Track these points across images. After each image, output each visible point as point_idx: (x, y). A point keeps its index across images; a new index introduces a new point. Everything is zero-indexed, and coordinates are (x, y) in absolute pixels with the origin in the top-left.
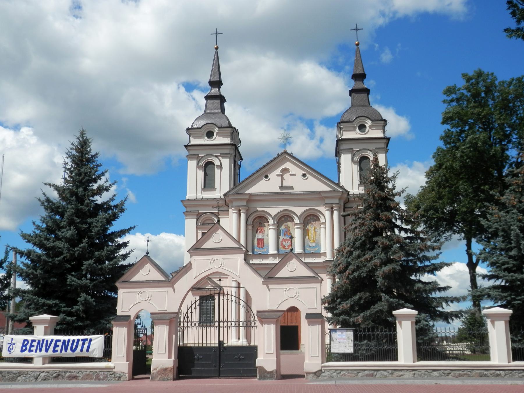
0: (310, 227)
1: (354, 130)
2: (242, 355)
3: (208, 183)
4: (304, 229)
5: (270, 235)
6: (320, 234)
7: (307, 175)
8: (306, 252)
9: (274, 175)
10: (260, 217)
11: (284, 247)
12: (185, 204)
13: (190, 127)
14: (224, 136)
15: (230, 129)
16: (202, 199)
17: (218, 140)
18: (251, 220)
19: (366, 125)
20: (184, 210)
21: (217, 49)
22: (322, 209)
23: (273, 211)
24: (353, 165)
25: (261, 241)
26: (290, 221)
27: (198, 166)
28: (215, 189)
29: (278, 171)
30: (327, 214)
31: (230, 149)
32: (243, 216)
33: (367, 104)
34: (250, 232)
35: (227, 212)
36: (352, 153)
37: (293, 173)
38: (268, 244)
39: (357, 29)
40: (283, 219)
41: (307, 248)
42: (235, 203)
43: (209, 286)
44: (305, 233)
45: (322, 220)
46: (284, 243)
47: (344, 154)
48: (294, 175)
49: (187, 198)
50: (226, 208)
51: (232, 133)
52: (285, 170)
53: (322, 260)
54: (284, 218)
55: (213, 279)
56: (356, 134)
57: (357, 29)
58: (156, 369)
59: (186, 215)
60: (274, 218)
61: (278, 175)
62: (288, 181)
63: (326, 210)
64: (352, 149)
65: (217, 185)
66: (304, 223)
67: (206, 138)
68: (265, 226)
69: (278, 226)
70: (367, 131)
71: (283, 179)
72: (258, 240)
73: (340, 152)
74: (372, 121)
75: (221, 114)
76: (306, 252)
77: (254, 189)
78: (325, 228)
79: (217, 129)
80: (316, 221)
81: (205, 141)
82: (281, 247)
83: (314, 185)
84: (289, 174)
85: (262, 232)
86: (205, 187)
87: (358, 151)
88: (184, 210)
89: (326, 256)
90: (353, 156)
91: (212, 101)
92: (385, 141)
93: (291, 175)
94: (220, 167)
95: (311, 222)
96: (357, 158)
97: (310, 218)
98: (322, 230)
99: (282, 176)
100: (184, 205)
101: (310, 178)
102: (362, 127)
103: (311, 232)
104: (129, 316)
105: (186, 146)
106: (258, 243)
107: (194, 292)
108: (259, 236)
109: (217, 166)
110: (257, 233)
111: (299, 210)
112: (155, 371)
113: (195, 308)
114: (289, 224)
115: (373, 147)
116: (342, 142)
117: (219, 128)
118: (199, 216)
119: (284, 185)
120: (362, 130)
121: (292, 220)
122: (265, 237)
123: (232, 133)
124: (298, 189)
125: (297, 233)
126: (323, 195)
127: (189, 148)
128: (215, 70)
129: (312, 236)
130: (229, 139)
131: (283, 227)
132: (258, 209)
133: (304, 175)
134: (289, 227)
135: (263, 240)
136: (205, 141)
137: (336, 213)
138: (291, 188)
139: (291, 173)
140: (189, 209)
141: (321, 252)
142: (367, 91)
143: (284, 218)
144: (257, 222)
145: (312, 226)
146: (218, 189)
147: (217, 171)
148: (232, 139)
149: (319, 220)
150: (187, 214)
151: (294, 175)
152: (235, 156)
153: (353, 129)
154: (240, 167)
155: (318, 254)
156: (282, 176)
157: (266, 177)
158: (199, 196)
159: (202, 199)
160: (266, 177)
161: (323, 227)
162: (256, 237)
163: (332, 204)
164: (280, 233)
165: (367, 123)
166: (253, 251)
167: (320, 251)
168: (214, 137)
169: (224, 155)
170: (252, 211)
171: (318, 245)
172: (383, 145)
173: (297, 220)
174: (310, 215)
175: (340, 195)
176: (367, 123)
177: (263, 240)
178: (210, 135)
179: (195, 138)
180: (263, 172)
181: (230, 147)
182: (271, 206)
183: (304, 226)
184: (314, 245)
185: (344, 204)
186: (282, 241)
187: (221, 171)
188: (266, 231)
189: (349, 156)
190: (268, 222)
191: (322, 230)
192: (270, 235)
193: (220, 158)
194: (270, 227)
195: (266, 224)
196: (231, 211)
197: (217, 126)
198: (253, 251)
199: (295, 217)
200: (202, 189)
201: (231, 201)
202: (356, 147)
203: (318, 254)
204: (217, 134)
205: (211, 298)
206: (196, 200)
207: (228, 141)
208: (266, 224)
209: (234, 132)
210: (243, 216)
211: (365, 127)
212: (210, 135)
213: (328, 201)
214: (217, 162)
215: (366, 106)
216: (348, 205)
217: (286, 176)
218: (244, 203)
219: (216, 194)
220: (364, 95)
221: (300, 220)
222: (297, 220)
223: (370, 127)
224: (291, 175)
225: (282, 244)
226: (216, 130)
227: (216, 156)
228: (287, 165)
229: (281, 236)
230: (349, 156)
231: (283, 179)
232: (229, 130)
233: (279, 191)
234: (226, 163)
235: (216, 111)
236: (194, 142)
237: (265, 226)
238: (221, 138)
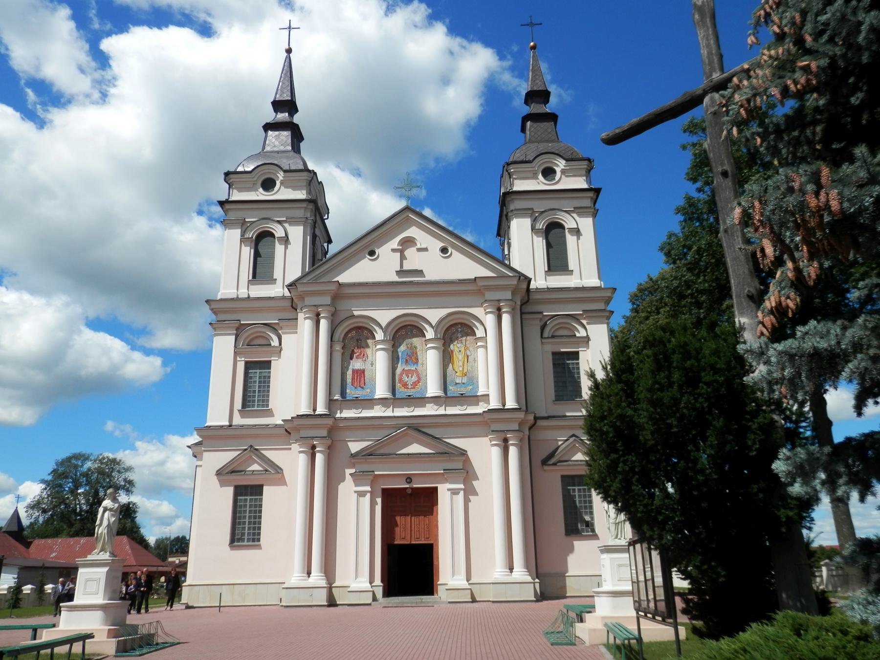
0: (455, 347)
1: (535, 177)
4: (444, 351)
5: (377, 362)
6: (475, 360)
7: (450, 250)
8: (449, 395)
9: (387, 252)
10: (360, 328)
11: (405, 385)
12: (213, 307)
13: (232, 170)
14: (295, 188)
15: (306, 174)
16: (249, 297)
17: (282, 193)
18: (339, 334)
19: (555, 168)
20: (213, 318)
21: (289, 51)
22: (478, 312)
23: (384, 316)
24: (535, 237)
25: (360, 374)
26: (417, 336)
27: (243, 240)
28: (273, 281)
29: (394, 243)
30: (490, 320)
31: (305, 208)
32: (324, 324)
33: (554, 138)
34: (338, 357)
35: (292, 322)
36: (531, 217)
37: (424, 246)
38: (373, 379)
40: (403, 332)
41: (450, 388)
42: (309, 301)
43: (255, 467)
44: (446, 358)
45: (480, 333)
46: (405, 378)
47: (516, 217)
48: (426, 249)
49: (219, 297)
50: (290, 315)
51: (311, 181)
52: (409, 242)
53: (479, 409)
54: (405, 331)
55: (263, 452)
56: (539, 184)
59: (215, 329)
60: (385, 330)
61: (394, 250)
62: (414, 260)
63: (486, 313)
64: (532, 209)
66: (444, 338)
67: (261, 190)
68: (368, 346)
69: (393, 346)
70: (557, 178)
71: (403, 258)
72: (354, 371)
73: (510, 214)
74: (567, 160)
75: (292, 153)
76: (449, 395)
77: (345, 277)
78: (486, 347)
79: (282, 173)
80: (467, 335)
81: (260, 195)
82: (398, 385)
83: (463, 267)
84: (414, 249)
85: (363, 357)
86: (254, 276)
87: (543, 212)
88: (213, 318)
89: (488, 402)
90: (534, 221)
91: (277, 133)
92: (591, 194)
93: (419, 250)
94: (286, 240)
95: (457, 338)
96: (541, 225)
97: (456, 330)
98: (481, 351)
99: (402, 252)
100: (212, 309)
101: (456, 255)
102: (549, 173)
103: (458, 357)
105: (222, 203)
106: (353, 379)
107: (222, 478)
108: (356, 364)
109: (280, 239)
110: (351, 358)
111: (434, 315)
114: (416, 341)
115: (569, 205)
116: (513, 197)
117: (285, 171)
118: (240, 329)
119: (406, 267)
120: (550, 177)
121: (421, 333)
122: (367, 367)
123: (311, 181)
124: (431, 275)
125: (431, 359)
127: (227, 206)
128: (283, 83)
129: (461, 364)
130: (304, 192)
131: (402, 348)
132: (356, 313)
133: (444, 250)
134: (416, 348)
135: (363, 371)
136: (260, 195)
137: (506, 319)
138: (420, 273)
139: (419, 246)
140: (222, 317)
141: (479, 394)
142: (552, 118)
143: (405, 331)
144: (351, 338)
145: (459, 345)
146: (279, 282)
147: (279, 248)
148: (309, 192)
149: (474, 334)
150: (218, 326)
151: (426, 249)
152: (315, 223)
153: (531, 175)
155: (475, 399)
156: (402, 252)
157: (372, 253)
158: (243, 293)
159: (249, 297)
160: (372, 253)
161: (482, 346)
162: (351, 367)
164: (398, 358)
165: (557, 165)
166: (343, 393)
167: (477, 392)
168: (276, 189)
169: (293, 221)
170: (342, 315)
171: (473, 381)
172: (587, 203)
173: (430, 334)
174: (452, 326)
175: (515, 283)
176: (557, 165)
177: (363, 371)
178: (268, 184)
179: (240, 190)
180: (367, 244)
181: (304, 205)
182: (380, 307)
183: (444, 345)
184: (465, 381)
185: (521, 305)
186: (401, 375)
187: (286, 248)
188: (370, 355)
189: (527, 222)
190: (374, 338)
191: (481, 351)
192: (377, 362)
193: (286, 225)
194: (378, 347)
195: (370, 342)
196: (301, 316)
197: (281, 168)
198: (343, 393)
199: (427, 326)
201: (302, 298)
202: (539, 205)
203: (475, 399)
204: (282, 183)
205: (257, 490)
206: (237, 299)
207: (301, 195)
208: (370, 342)
209: (313, 182)
210: (324, 324)
211: (554, 172)
212: (268, 184)
213: (489, 295)
214: (279, 232)
215: (553, 141)
216: (529, 308)
217: (410, 252)
218: (327, 300)
219: (277, 290)
220: (548, 125)
221: (436, 332)
222: (430, 334)
223: (563, 172)
224: (419, 250)
225: (401, 380)
226: (281, 176)
227: (279, 222)
228: (413, 232)
229: (399, 365)
230: (527, 222)
231: (403, 258)
232: (305, 176)
233: (396, 279)
234: (297, 233)
235: (282, 148)
236: (236, 196)
237: (368, 346)
238: (290, 190)
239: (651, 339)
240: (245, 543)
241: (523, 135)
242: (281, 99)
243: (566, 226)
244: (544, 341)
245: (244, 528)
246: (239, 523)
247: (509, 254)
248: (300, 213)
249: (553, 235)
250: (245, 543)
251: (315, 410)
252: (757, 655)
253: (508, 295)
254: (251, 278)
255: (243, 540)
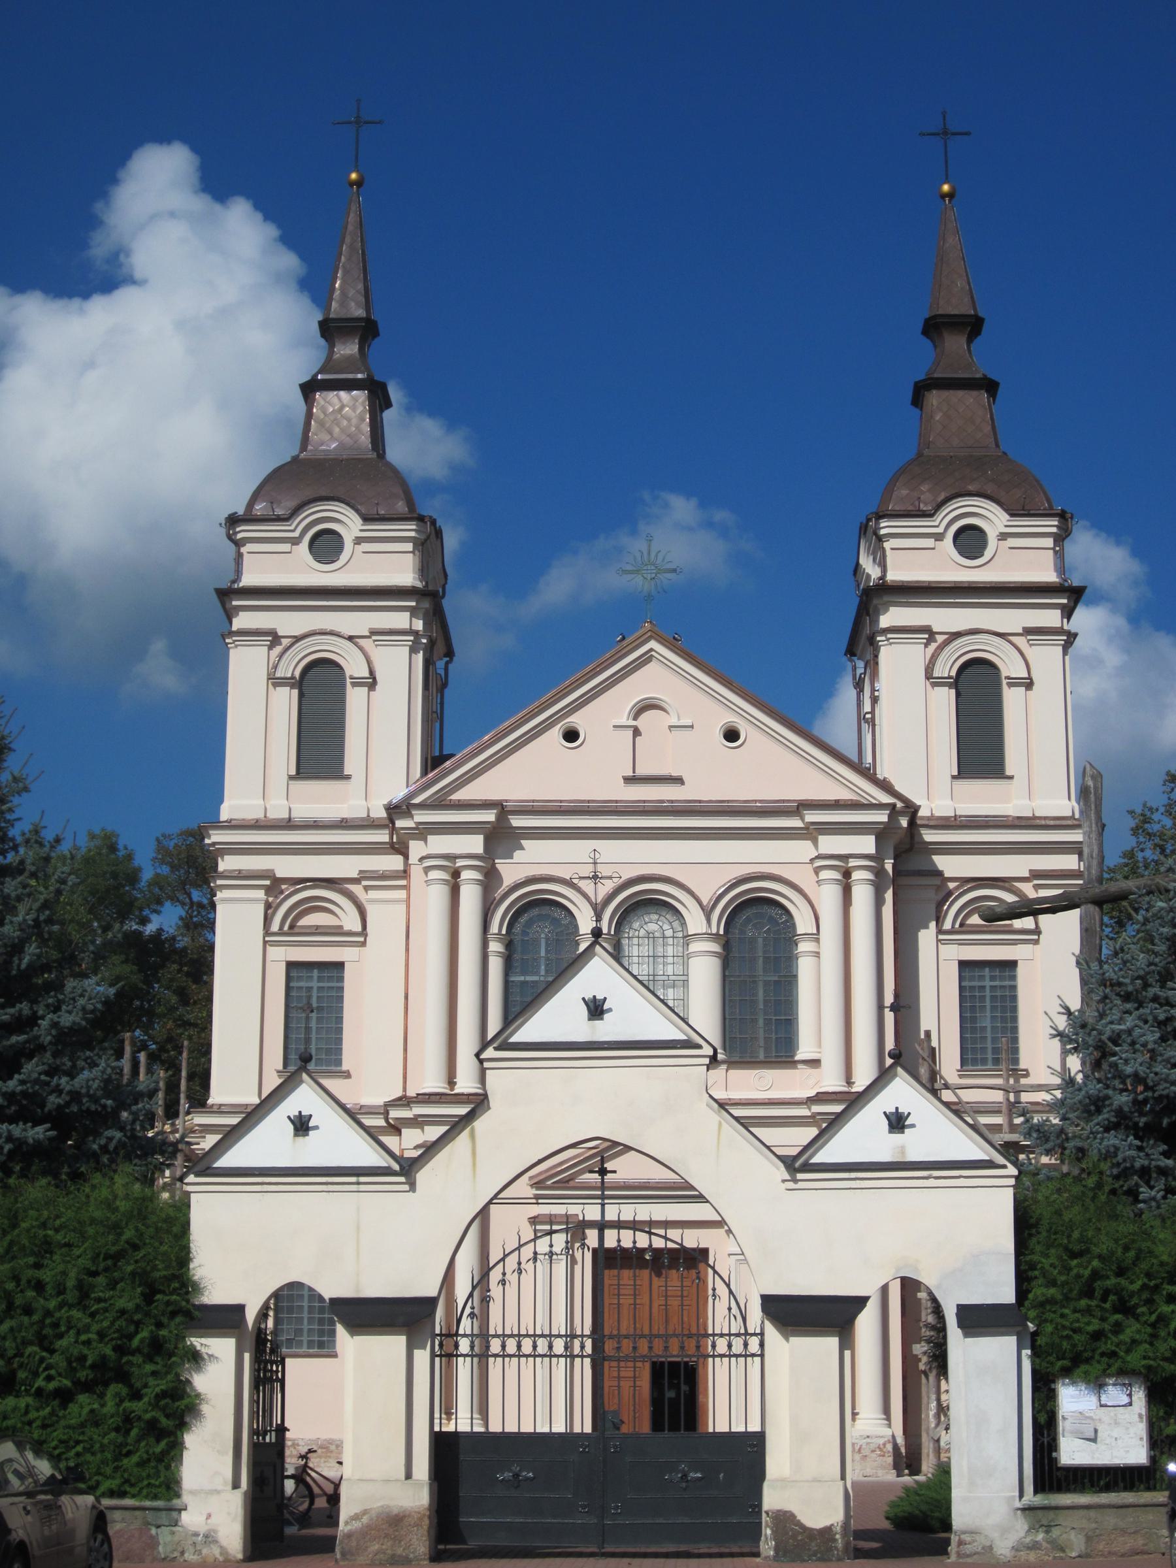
2: (695, 1467)
3: (319, 750)
13: (241, 511)
30: (828, 897)
39: (945, 132)
42: (440, 844)
57: (945, 132)
58: (356, 1517)
65: (353, 761)
96: (946, 667)
104: (240, 1309)
112: (356, 1525)
113: (503, 1282)
116: (886, 598)
126: (812, 817)
154: (445, 685)
163: (845, 858)
168: (344, 557)
200: (291, 778)
218: (475, 844)
239: (1107, 1103)
240: (304, 1350)
241: (918, 411)
242: (343, 315)
243: (1004, 673)
244: (941, 937)
245: (300, 1320)
246: (290, 1310)
247: (873, 712)
248: (401, 620)
249: (977, 694)
250: (304, 1350)
251: (451, 1083)
252: (6, 1326)
253: (867, 844)
254: (293, 772)
255: (300, 1344)
